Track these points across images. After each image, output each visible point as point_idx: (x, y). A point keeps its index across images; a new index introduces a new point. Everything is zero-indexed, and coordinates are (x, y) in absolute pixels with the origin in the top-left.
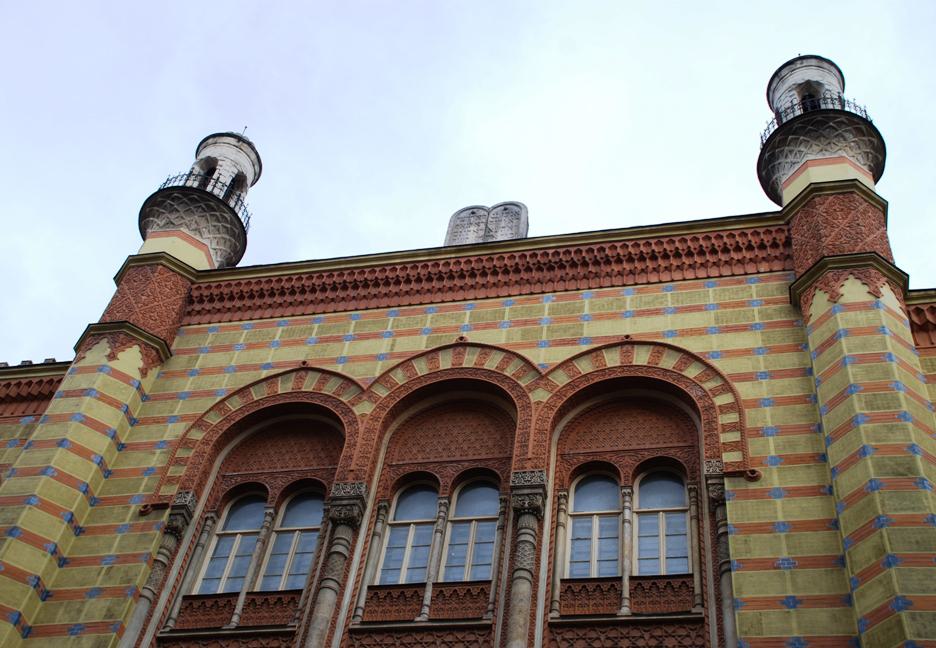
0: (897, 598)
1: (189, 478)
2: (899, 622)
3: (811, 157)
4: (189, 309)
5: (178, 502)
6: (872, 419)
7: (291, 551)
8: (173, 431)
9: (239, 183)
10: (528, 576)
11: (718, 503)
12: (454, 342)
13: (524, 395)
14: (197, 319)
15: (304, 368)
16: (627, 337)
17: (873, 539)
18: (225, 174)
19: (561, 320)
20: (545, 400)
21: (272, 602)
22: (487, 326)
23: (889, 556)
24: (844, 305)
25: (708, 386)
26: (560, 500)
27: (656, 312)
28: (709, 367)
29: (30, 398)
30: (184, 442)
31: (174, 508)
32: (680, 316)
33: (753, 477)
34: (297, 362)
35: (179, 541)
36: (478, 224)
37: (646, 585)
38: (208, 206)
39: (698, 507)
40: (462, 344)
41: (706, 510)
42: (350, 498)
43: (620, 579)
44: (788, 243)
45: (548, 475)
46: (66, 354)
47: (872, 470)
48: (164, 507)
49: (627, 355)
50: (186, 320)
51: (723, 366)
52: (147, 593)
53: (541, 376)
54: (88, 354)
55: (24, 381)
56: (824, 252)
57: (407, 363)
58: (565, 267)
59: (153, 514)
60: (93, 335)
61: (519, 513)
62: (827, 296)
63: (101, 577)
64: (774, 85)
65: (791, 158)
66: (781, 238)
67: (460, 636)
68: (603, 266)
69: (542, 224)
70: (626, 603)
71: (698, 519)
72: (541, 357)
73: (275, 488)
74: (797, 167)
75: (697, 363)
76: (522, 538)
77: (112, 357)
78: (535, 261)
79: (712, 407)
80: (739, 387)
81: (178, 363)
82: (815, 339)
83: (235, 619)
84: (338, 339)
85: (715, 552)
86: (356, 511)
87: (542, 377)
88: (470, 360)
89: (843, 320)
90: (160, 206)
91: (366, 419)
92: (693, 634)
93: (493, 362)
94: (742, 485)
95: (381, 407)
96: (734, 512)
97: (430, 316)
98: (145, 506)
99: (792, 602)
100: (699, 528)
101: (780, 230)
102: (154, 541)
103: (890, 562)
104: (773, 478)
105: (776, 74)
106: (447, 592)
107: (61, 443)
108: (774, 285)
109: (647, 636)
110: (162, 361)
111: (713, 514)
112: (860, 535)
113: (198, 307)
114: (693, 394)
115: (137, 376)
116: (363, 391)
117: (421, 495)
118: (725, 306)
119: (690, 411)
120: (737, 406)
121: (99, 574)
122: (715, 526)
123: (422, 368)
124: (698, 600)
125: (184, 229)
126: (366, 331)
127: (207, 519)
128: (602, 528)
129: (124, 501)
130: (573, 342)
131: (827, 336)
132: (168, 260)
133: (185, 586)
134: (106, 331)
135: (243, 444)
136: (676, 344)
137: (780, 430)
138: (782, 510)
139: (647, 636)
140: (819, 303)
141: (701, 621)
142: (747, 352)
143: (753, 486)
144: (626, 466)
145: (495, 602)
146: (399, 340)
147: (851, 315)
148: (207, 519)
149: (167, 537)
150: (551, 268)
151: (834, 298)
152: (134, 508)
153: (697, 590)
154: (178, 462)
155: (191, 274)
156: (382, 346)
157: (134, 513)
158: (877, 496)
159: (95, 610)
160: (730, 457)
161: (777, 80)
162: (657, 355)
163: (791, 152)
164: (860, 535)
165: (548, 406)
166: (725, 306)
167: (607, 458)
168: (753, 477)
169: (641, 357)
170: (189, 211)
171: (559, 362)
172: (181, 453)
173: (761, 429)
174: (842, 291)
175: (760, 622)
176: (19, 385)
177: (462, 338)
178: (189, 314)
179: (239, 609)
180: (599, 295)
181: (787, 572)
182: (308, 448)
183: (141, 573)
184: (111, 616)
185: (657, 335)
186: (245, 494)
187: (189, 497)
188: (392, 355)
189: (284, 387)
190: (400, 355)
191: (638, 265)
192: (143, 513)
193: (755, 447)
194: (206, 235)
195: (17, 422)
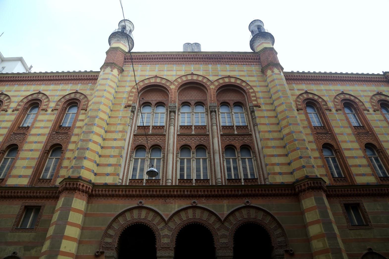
0: (292, 131)
1: (134, 100)
2: (293, 135)
3: (263, 41)
4: (125, 61)
5: (133, 105)
6: (284, 97)
7: (30, 118)
8: (128, 89)
9: (131, 31)
10: (215, 124)
11: (253, 112)
12: (190, 73)
13: (209, 86)
14: (127, 63)
15: (156, 77)
16: (229, 76)
17: (286, 120)
18: (128, 28)
20: (214, 88)
21: (197, 128)
23: (290, 123)
24: (275, 73)
25: (248, 87)
26: (179, 109)
27: (234, 71)
28: (247, 83)
29: (92, 79)
30: (131, 92)
31: (132, 106)
32: (239, 72)
33: (260, 107)
34: (154, 75)
35: (134, 114)
36: (190, 47)
37: (239, 127)
38: (123, 35)
39: (167, 112)
40: (192, 74)
41: (249, 113)
42: (173, 107)
43: (233, 126)
44: (259, 59)
45: (136, 104)
46: (99, 70)
47: (285, 107)
48: (130, 106)
49: (156, 79)
50: (125, 63)
51: (251, 84)
52: (130, 125)
53: (212, 83)
54: (106, 70)
55: (88, 75)
56: (269, 62)
57: (180, 77)
58: (213, 59)
59: (128, 108)
60: (106, 66)
61: (211, 112)
62: (271, 71)
63: (119, 121)
64: (251, 25)
65: (258, 41)
66: (258, 58)
67: (140, 136)
68: (224, 60)
69: (205, 48)
70: (236, 131)
71: (248, 114)
72: (212, 78)
73: (154, 103)
74: (260, 43)
75: (244, 83)
76: (171, 117)
77: (112, 71)
78: (182, 57)
79: (249, 92)
80: (254, 88)
81: (125, 73)
82: (269, 80)
83: (150, 131)
84: (163, 71)
85: (169, 121)
86: (175, 109)
87: (212, 83)
88: (195, 78)
89: (275, 77)
90: (113, 36)
91: (174, 89)
92: (250, 137)
93: (200, 79)
94: (258, 108)
95: (176, 87)
96: (257, 114)
97: (148, 67)
98: (126, 106)
99: (269, 132)
100: (167, 116)
101: (257, 56)
102: (129, 114)
103: (290, 124)
104: (263, 107)
105: (252, 22)
106: (155, 128)
107: (105, 90)
108: (257, 67)
109: (198, 137)
110: (121, 73)
111: (251, 114)
112: (283, 119)
113: (127, 60)
114: (245, 89)
115: (117, 76)
116: (172, 83)
117: (187, 107)
118: (248, 71)
119: (167, 92)
120: (254, 92)
121: (119, 120)
122: (252, 117)
123: (184, 79)
124: (165, 131)
125: (122, 42)
126: (169, 69)
127: (138, 109)
128: (227, 115)
129: (120, 104)
130: (217, 76)
131: (272, 79)
132: (120, 49)
133: (137, 124)
134: (106, 65)
135: (143, 93)
136: (240, 78)
137: (264, 98)
138: (266, 114)
139: (198, 137)
140: (269, 72)
141: (251, 135)
142: (254, 81)
143: (260, 109)
144: (231, 103)
145: (166, 130)
146: (178, 72)
147: (277, 76)
148: (138, 109)
149: (132, 113)
150: (210, 59)
151: (273, 72)
152: (123, 106)
153: (165, 129)
154: (131, 96)
155: (125, 52)
156: (174, 73)
157: (123, 107)
158: (286, 112)
159: (120, 128)
160: (255, 103)
161: (251, 24)
162: (161, 80)
163: (258, 40)
164: (283, 119)
165: (214, 89)
166: (248, 71)
167: (227, 101)
168: (260, 107)
169: (233, 80)
170: (122, 38)
171: (215, 80)
172: (131, 94)
173: (259, 97)
174: (274, 70)
175: (264, 135)
176: (79, 76)
177: (192, 73)
178: (125, 62)
179: (151, 129)
180: (221, 66)
181: (268, 126)
182: (159, 95)
183: (128, 120)
184: (124, 129)
186: (147, 104)
187: (135, 105)
188: (177, 75)
189: (153, 81)
190: (179, 75)
191: (229, 60)
192: (126, 107)
193: (259, 101)
194: (126, 44)
195: (88, 85)
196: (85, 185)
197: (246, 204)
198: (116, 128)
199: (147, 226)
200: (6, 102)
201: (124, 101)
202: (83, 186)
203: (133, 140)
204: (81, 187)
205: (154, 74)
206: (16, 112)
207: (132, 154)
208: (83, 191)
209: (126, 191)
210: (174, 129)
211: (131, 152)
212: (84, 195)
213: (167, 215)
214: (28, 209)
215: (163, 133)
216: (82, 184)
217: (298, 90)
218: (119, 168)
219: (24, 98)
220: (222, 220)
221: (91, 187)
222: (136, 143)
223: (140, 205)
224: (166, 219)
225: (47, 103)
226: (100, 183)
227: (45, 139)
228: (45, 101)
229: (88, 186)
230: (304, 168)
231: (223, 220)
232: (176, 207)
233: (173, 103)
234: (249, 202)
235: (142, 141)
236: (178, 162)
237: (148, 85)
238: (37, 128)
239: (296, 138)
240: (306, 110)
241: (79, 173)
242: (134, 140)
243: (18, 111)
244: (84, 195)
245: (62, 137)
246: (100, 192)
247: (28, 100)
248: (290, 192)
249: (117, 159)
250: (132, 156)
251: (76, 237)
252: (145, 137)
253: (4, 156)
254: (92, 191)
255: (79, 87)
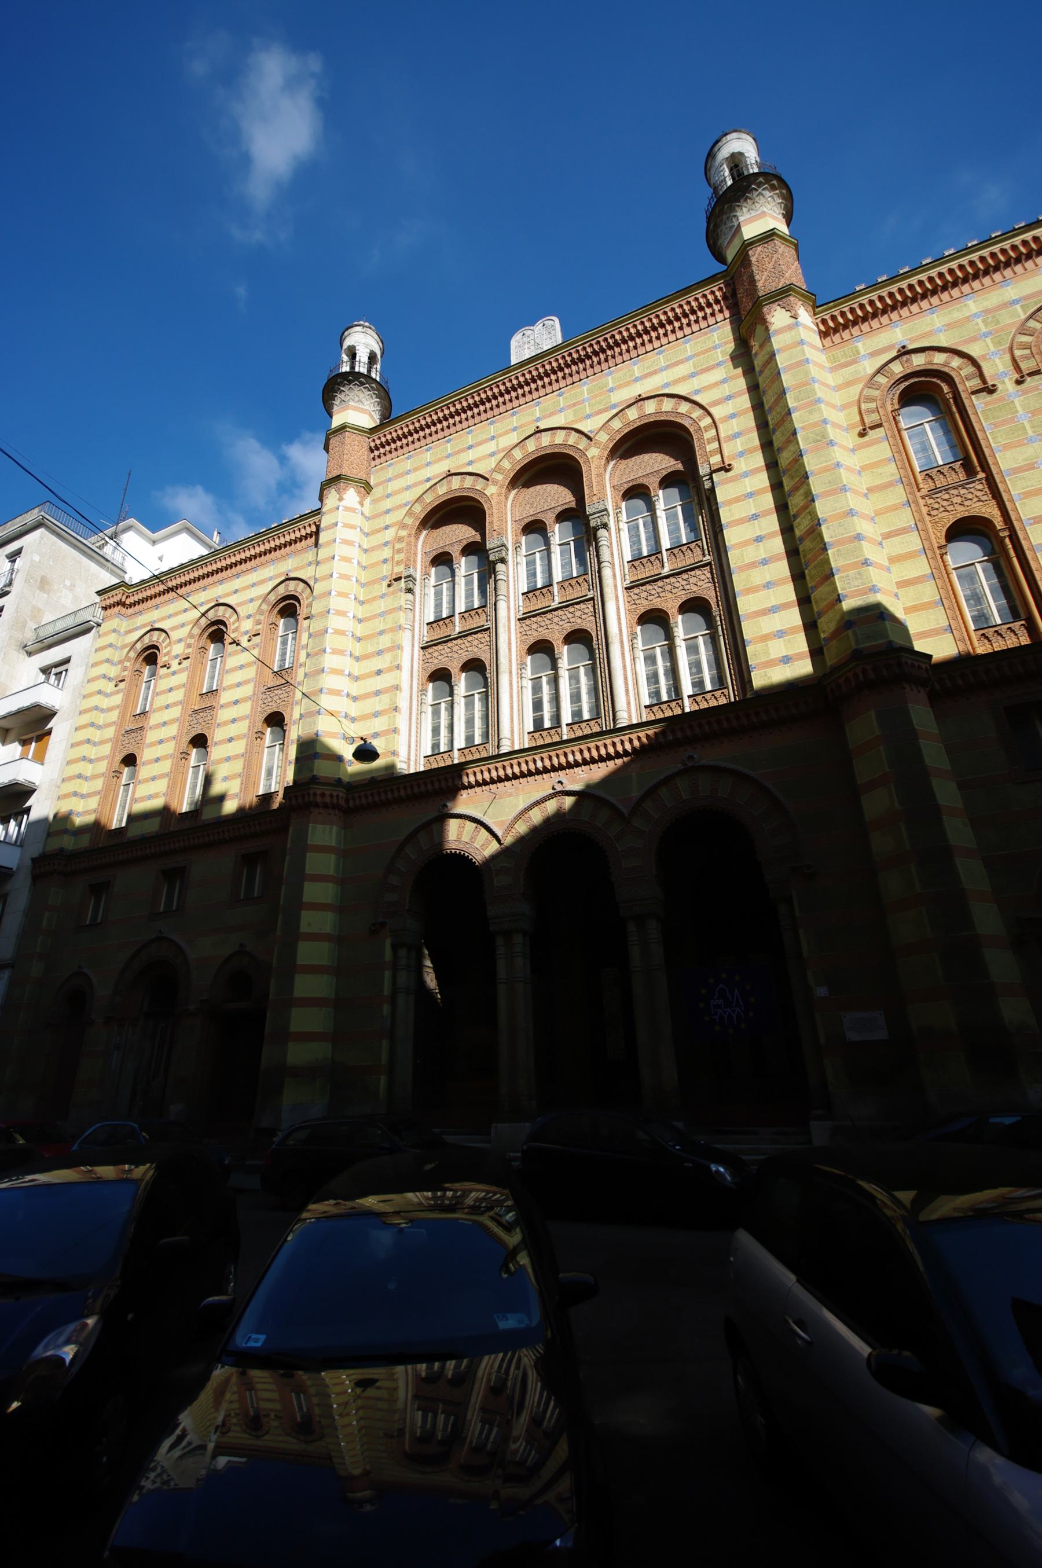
1: (408, 559)
12: (533, 432)
16: (640, 396)
19: (596, 396)
20: (596, 454)
22: (552, 414)
40: (539, 431)
48: (399, 579)
49: (641, 408)
113: (376, 453)
115: (359, 507)
121: (380, 623)
125: (352, 403)
130: (606, 410)
177: (538, 427)
185: (658, 389)
190: (503, 450)
194: (366, 403)
196: (327, 793)
197: (686, 764)
198: (378, 643)
199: (464, 854)
200: (164, 645)
201: (385, 570)
202: (323, 795)
203: (421, 662)
204: (319, 799)
205: (442, 468)
206: (122, 685)
207: (424, 697)
208: (326, 806)
209: (412, 787)
210: (509, 608)
211: (421, 691)
212: (329, 814)
213: (503, 822)
214: (249, 860)
215: (660, 574)
216: (319, 792)
217: (873, 354)
218: (394, 738)
219: (193, 627)
220: (624, 814)
221: (341, 795)
222: (428, 667)
223: (690, 764)
224: (625, 811)
225: (236, 625)
226: (362, 780)
227: (109, 749)
228: (231, 620)
229: (335, 794)
230: (849, 628)
231: (627, 815)
232: (521, 802)
233: (495, 536)
234: (695, 756)
235: (442, 658)
236: (637, 660)
237: (433, 506)
238: (231, 687)
239: (831, 537)
240: (896, 423)
241: (312, 770)
242: (632, 602)
243: (189, 660)
244: (320, 813)
245: (967, 499)
246: (364, 801)
247: (200, 629)
248: (396, 794)
249: (389, 717)
250: (423, 701)
251: (329, 901)
252: (486, 636)
253: (121, 781)
254: (347, 800)
255: (290, 564)
